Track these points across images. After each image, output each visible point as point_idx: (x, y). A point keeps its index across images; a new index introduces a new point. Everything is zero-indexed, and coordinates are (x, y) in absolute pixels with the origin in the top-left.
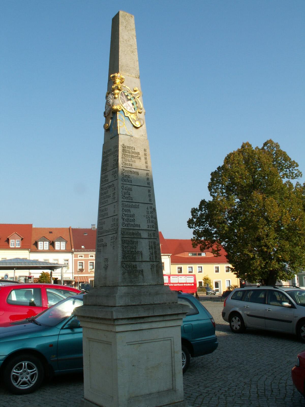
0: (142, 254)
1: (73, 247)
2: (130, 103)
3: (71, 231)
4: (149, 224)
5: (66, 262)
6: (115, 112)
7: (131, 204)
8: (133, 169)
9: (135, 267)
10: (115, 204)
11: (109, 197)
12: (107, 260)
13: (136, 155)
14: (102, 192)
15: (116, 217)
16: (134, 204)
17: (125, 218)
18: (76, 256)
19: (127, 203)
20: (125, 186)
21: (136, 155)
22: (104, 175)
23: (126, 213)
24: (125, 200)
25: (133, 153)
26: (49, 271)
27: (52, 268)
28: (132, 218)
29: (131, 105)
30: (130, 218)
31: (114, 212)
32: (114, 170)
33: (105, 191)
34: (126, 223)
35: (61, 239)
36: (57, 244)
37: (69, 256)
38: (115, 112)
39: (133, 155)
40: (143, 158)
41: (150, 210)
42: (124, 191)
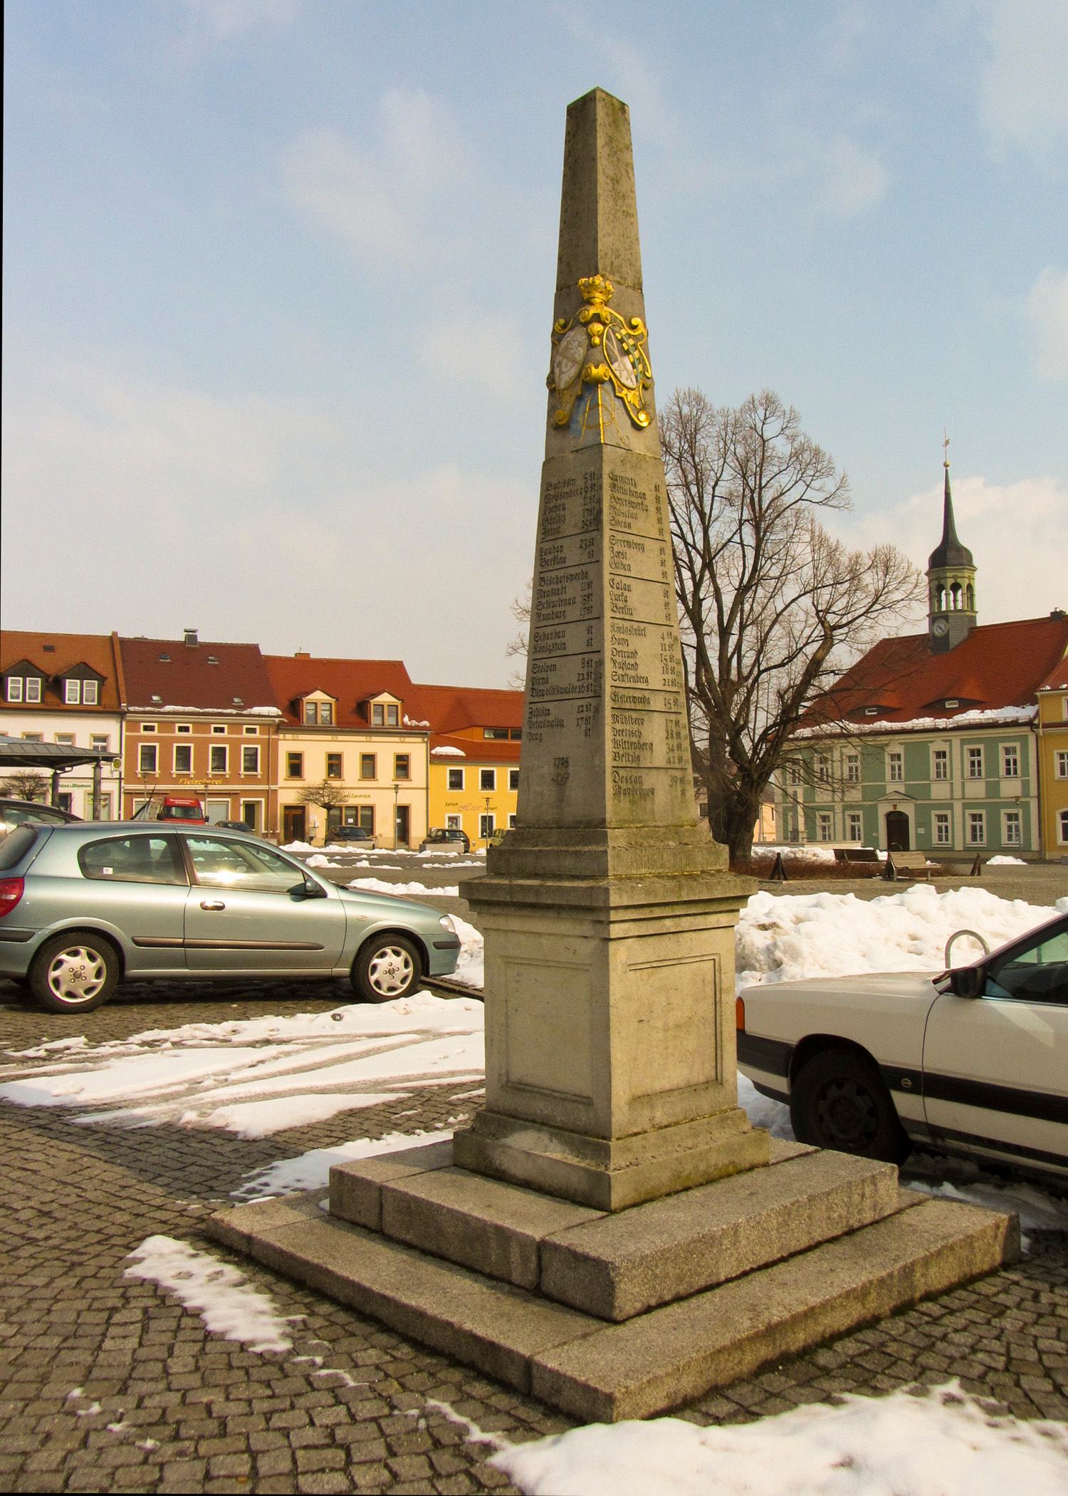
0: (651, 749)
1: (123, 696)
2: (627, 361)
3: (117, 647)
4: (666, 677)
5: (100, 744)
6: (590, 385)
7: (628, 624)
8: (632, 537)
9: (638, 780)
10: (594, 623)
11: (571, 602)
12: (564, 762)
13: (639, 501)
14: (545, 588)
15: (595, 657)
16: (636, 625)
17: (619, 659)
18: (133, 726)
19: (621, 623)
20: (617, 579)
21: (639, 501)
22: (546, 546)
23: (619, 648)
24: (618, 616)
25: (632, 494)
26: (47, 772)
27: (60, 761)
28: (632, 661)
29: (630, 367)
30: (628, 661)
31: (589, 643)
32: (587, 536)
33: (555, 586)
34: (620, 672)
35: (83, 671)
36: (72, 688)
37: (110, 727)
38: (590, 385)
39: (633, 499)
40: (652, 509)
41: (668, 641)
42: (616, 592)
